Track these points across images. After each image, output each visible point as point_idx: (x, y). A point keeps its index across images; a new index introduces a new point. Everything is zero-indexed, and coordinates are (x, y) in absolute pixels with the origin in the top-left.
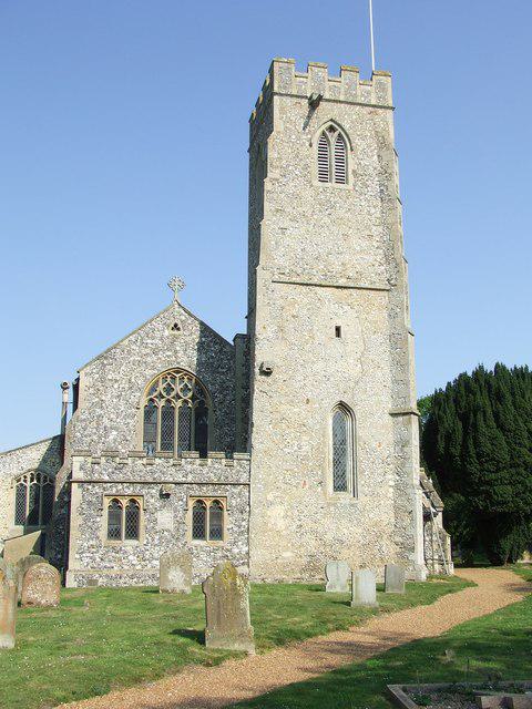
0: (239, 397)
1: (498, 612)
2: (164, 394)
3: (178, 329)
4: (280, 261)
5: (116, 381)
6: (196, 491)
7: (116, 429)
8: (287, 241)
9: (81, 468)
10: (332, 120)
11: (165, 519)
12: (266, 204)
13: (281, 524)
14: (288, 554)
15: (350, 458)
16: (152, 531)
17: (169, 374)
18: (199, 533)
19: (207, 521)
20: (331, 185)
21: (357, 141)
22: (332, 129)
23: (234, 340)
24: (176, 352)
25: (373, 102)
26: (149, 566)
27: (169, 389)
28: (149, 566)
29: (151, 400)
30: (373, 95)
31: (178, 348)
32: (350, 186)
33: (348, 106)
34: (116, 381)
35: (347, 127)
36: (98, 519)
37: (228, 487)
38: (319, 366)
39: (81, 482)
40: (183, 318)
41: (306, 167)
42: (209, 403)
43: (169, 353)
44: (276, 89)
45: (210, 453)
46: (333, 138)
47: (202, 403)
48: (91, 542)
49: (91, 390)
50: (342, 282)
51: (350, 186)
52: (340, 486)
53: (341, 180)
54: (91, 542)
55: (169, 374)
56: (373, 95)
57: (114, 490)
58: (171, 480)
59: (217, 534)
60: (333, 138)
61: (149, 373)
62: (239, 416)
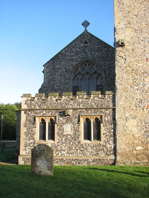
3: (87, 43)
5: (60, 69)
9: (25, 104)
11: (68, 129)
13: (135, 130)
16: (61, 135)
17: (83, 63)
18: (88, 136)
19: (92, 130)
23: (114, 46)
24: (86, 53)
26: (60, 154)
28: (60, 154)
29: (76, 76)
31: (87, 51)
34: (60, 69)
36: (34, 129)
37: (103, 110)
39: (26, 111)
40: (89, 38)
43: (84, 54)
45: (92, 92)
48: (31, 141)
49: (49, 74)
54: (31, 141)
55: (83, 63)
57: (42, 114)
58: (71, 107)
59: (98, 137)
61: (74, 63)
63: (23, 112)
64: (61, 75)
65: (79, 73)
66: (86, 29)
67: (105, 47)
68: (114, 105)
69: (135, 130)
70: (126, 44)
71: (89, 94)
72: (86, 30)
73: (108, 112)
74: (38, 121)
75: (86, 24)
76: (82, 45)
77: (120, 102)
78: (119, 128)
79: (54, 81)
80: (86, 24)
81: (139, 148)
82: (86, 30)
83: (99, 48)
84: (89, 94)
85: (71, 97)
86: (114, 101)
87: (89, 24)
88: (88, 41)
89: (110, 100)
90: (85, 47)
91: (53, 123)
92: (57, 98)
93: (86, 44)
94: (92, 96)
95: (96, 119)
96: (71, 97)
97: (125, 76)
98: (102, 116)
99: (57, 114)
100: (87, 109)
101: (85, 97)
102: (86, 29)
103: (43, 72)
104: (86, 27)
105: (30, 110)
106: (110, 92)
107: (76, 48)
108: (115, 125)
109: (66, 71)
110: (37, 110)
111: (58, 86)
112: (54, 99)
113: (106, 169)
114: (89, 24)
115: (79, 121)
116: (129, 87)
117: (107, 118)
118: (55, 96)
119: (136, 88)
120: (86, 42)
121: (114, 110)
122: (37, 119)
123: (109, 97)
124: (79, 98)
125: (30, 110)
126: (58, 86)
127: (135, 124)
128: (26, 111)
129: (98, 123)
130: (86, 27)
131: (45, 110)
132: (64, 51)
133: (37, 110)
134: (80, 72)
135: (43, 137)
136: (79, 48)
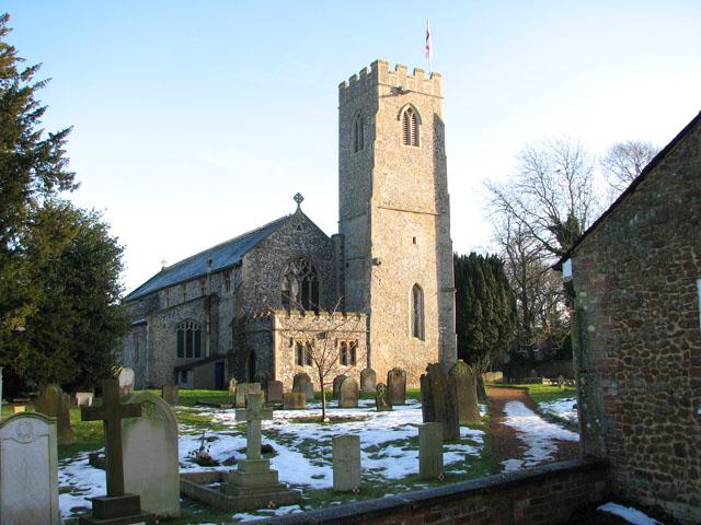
0: (338, 275)
12: (376, 158)
13: (386, 355)
18: (407, 143)
19: (348, 354)
22: (409, 110)
25: (433, 94)
38: (406, 261)
39: (281, 331)
41: (396, 135)
44: (380, 81)
46: (411, 119)
47: (315, 279)
50: (416, 209)
53: (416, 144)
60: (411, 119)
62: (338, 287)
68: (368, 329)
69: (386, 355)
72: (299, 209)
75: (299, 198)
78: (373, 353)
80: (299, 198)
82: (299, 209)
84: (317, 314)
86: (368, 325)
87: (302, 199)
91: (309, 346)
97: (379, 298)
103: (473, 254)
104: (299, 203)
112: (311, 319)
113: (374, 194)
114: (302, 199)
115: (292, 343)
117: (362, 343)
121: (368, 334)
130: (299, 203)
135: (300, 362)
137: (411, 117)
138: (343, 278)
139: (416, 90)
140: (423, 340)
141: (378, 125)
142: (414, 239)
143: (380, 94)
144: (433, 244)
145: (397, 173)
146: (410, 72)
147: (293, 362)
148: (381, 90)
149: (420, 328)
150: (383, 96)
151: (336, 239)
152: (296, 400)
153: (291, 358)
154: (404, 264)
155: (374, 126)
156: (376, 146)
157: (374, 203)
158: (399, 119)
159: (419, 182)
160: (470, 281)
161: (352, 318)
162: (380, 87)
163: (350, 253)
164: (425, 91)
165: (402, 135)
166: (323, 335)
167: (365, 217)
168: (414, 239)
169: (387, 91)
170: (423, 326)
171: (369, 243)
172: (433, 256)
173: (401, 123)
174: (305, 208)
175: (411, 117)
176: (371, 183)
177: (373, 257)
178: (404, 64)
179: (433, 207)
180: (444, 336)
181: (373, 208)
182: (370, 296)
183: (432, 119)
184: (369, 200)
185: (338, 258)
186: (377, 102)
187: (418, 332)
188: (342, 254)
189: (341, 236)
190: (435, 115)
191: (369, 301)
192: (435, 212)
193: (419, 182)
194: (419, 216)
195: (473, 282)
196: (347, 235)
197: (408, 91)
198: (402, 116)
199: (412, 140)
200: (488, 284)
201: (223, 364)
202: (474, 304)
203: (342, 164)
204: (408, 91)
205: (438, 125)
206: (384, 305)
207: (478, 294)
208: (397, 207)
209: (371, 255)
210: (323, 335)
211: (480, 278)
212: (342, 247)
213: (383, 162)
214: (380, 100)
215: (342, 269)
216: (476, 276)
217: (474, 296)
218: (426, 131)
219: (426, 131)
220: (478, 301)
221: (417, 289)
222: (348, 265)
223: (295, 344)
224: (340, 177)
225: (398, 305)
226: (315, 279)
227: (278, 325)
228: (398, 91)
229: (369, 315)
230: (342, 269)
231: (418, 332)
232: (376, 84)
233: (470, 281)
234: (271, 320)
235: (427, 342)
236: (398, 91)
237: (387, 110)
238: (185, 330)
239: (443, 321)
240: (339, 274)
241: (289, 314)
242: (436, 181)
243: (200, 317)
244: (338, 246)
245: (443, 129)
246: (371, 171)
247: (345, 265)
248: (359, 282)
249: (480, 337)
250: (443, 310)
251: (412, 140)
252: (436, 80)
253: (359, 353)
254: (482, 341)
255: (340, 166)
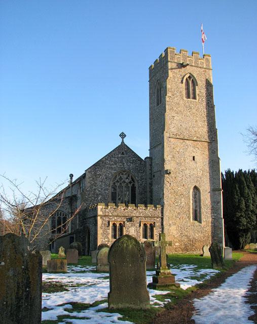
0: (148, 182)
1: (209, 152)
2: (119, 181)
4: (173, 130)
6: (144, 221)
7: (101, 195)
8: (175, 121)
10: (190, 74)
12: (167, 107)
13: (175, 232)
14: (177, 244)
15: (54, 280)
18: (188, 97)
19: (148, 230)
20: (191, 100)
21: (199, 82)
22: (189, 77)
25: (205, 67)
27: (121, 178)
30: (205, 64)
31: (124, 162)
32: (197, 101)
33: (196, 68)
35: (195, 76)
38: (187, 172)
39: (102, 217)
41: (181, 92)
42: (136, 185)
44: (169, 60)
46: (190, 82)
47: (133, 185)
49: (91, 179)
50: (195, 138)
51: (197, 101)
52: (195, 218)
53: (194, 98)
56: (205, 64)
60: (190, 82)
61: (113, 172)
62: (148, 190)
63: (99, 218)
64: (101, 182)
65: (118, 181)
66: (123, 140)
67: (139, 160)
68: (162, 215)
69: (175, 232)
70: (172, 173)
71: (146, 207)
72: (123, 142)
73: (158, 220)
74: (111, 224)
75: (123, 136)
76: (120, 155)
77: (167, 213)
79: (95, 186)
80: (123, 136)
81: (177, 244)
82: (123, 142)
83: (133, 160)
84: (146, 207)
85: (134, 208)
86: (162, 213)
87: (125, 136)
88: (124, 153)
89: (160, 212)
90: (123, 158)
92: (125, 208)
93: (123, 156)
94: (148, 208)
95: (120, 224)
96: (134, 208)
98: (155, 222)
99: (125, 220)
100: (145, 217)
101: (144, 208)
102: (123, 140)
104: (123, 138)
105: (105, 216)
106: (160, 206)
107: (115, 158)
108: (163, 229)
109: (106, 178)
110: (111, 216)
111: (99, 191)
114: (125, 136)
115: (140, 225)
116: (172, 203)
117: (158, 224)
118: (123, 207)
119: (176, 204)
120: (123, 154)
121: (162, 219)
122: (111, 223)
123: (159, 210)
124: (140, 209)
125: (105, 216)
126: (99, 191)
127: (175, 228)
128: (102, 217)
129: (152, 227)
130: (123, 138)
131: (117, 216)
132: (104, 159)
133: (111, 216)
134: (118, 181)
136: (118, 158)
137: (191, 82)
138: (151, 184)
139: (193, 64)
140: (200, 222)
141: (168, 86)
142: (194, 157)
143: (169, 68)
144: (207, 161)
145: (183, 116)
146: (200, 56)
147: (110, 236)
148: (170, 65)
149: (198, 214)
150: (172, 69)
151: (147, 160)
152: (59, 265)
153: (108, 234)
154: (187, 171)
155: (166, 87)
156: (167, 99)
157: (166, 135)
158: (182, 82)
159: (196, 121)
160: (237, 186)
161: (151, 208)
162: (169, 63)
163: (155, 169)
164: (200, 66)
165: (184, 92)
166: (130, 220)
167: (160, 146)
168: (194, 157)
169: (174, 65)
170: (200, 214)
171: (163, 160)
172: (207, 168)
173: (184, 85)
174: (127, 142)
175: (191, 82)
176: (164, 123)
177: (166, 169)
178: (185, 50)
179: (206, 137)
180: (215, 220)
181: (165, 138)
182: (163, 194)
183: (204, 83)
184: (163, 133)
185: (148, 172)
186: (168, 73)
187: (197, 217)
188: (151, 170)
189: (150, 158)
190: (206, 79)
191: (163, 197)
192: (208, 140)
193: (196, 121)
194: (196, 142)
195: (239, 187)
196: (153, 158)
197: (188, 65)
198: (184, 81)
199: (191, 95)
200: (248, 188)
201: (73, 237)
202: (240, 201)
203: (151, 114)
204: (188, 65)
205: (209, 85)
206: (173, 200)
207: (242, 195)
208: (182, 137)
209: (164, 168)
210: (130, 220)
211: (243, 184)
212: (151, 165)
213: (172, 109)
214: (169, 71)
215: (151, 179)
216: (241, 183)
217: (240, 195)
218: (201, 90)
219: (201, 90)
220: (242, 199)
221: (196, 188)
222: (154, 176)
223: (142, 225)
224: (150, 122)
225: (183, 200)
226: (133, 185)
227: (100, 213)
228: (182, 66)
229: (163, 207)
230: (151, 179)
231: (197, 217)
232: (167, 62)
233: (237, 186)
234: (96, 209)
235: (203, 223)
236: (182, 66)
237: (174, 77)
238: (62, 217)
239: (214, 210)
240: (149, 181)
241: (108, 206)
242: (208, 121)
243: (67, 209)
244: (148, 166)
245: (212, 88)
246: (164, 115)
247: (152, 176)
248: (159, 186)
249: (244, 221)
250: (215, 203)
251: (191, 95)
252: (207, 59)
253: (156, 232)
254: (245, 224)
255: (150, 116)
